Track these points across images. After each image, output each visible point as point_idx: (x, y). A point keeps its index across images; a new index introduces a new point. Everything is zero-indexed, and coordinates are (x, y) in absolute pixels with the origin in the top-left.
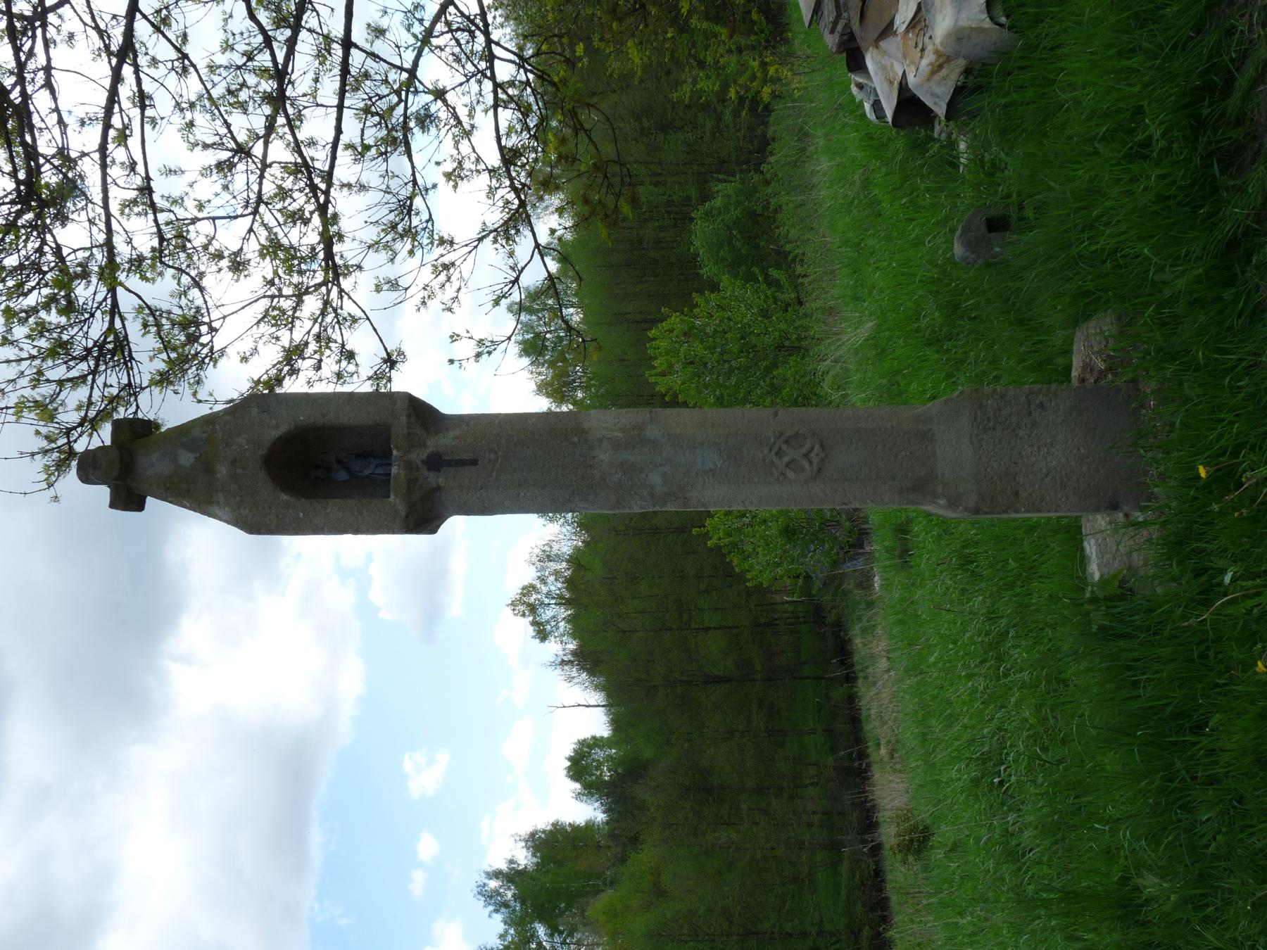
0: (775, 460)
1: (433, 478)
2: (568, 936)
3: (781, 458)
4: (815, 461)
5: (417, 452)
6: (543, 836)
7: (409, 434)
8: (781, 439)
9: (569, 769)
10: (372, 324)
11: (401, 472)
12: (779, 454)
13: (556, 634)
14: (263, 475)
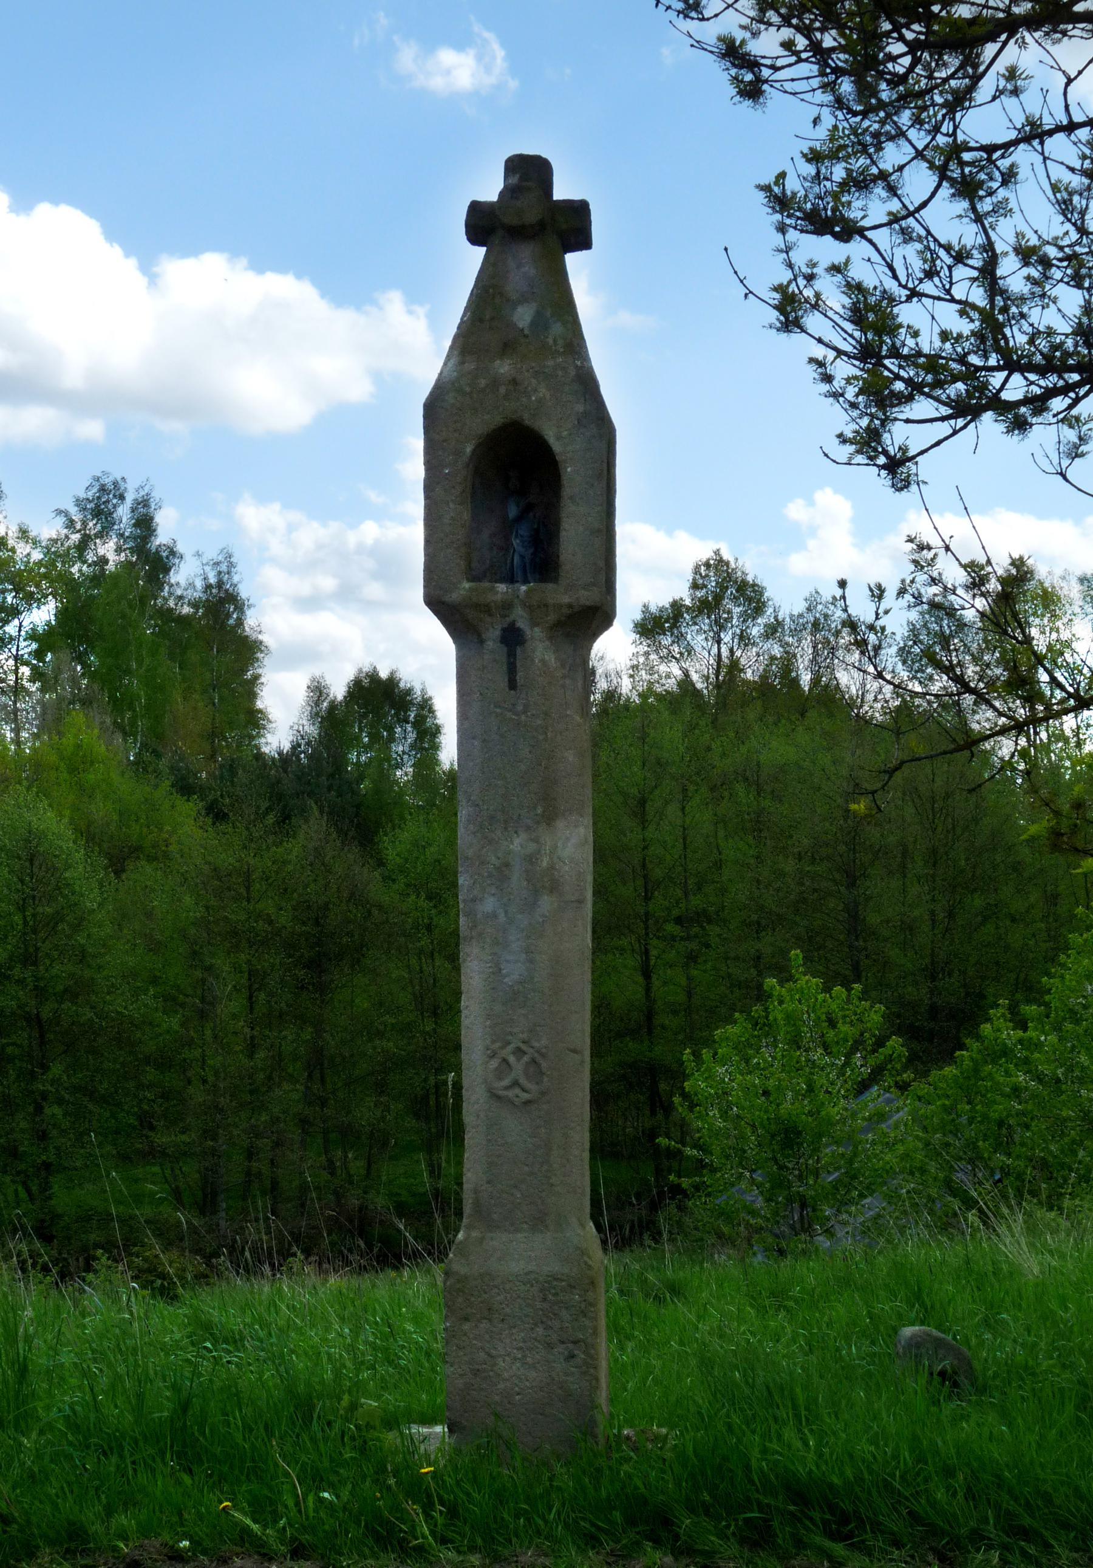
0: (510, 1048)
1: (493, 634)
2: (34, 669)
3: (514, 1053)
4: (510, 1094)
5: (525, 615)
6: (231, 622)
7: (546, 605)
8: (536, 1055)
9: (373, 676)
12: (519, 1052)
13: (653, 657)
14: (498, 420)
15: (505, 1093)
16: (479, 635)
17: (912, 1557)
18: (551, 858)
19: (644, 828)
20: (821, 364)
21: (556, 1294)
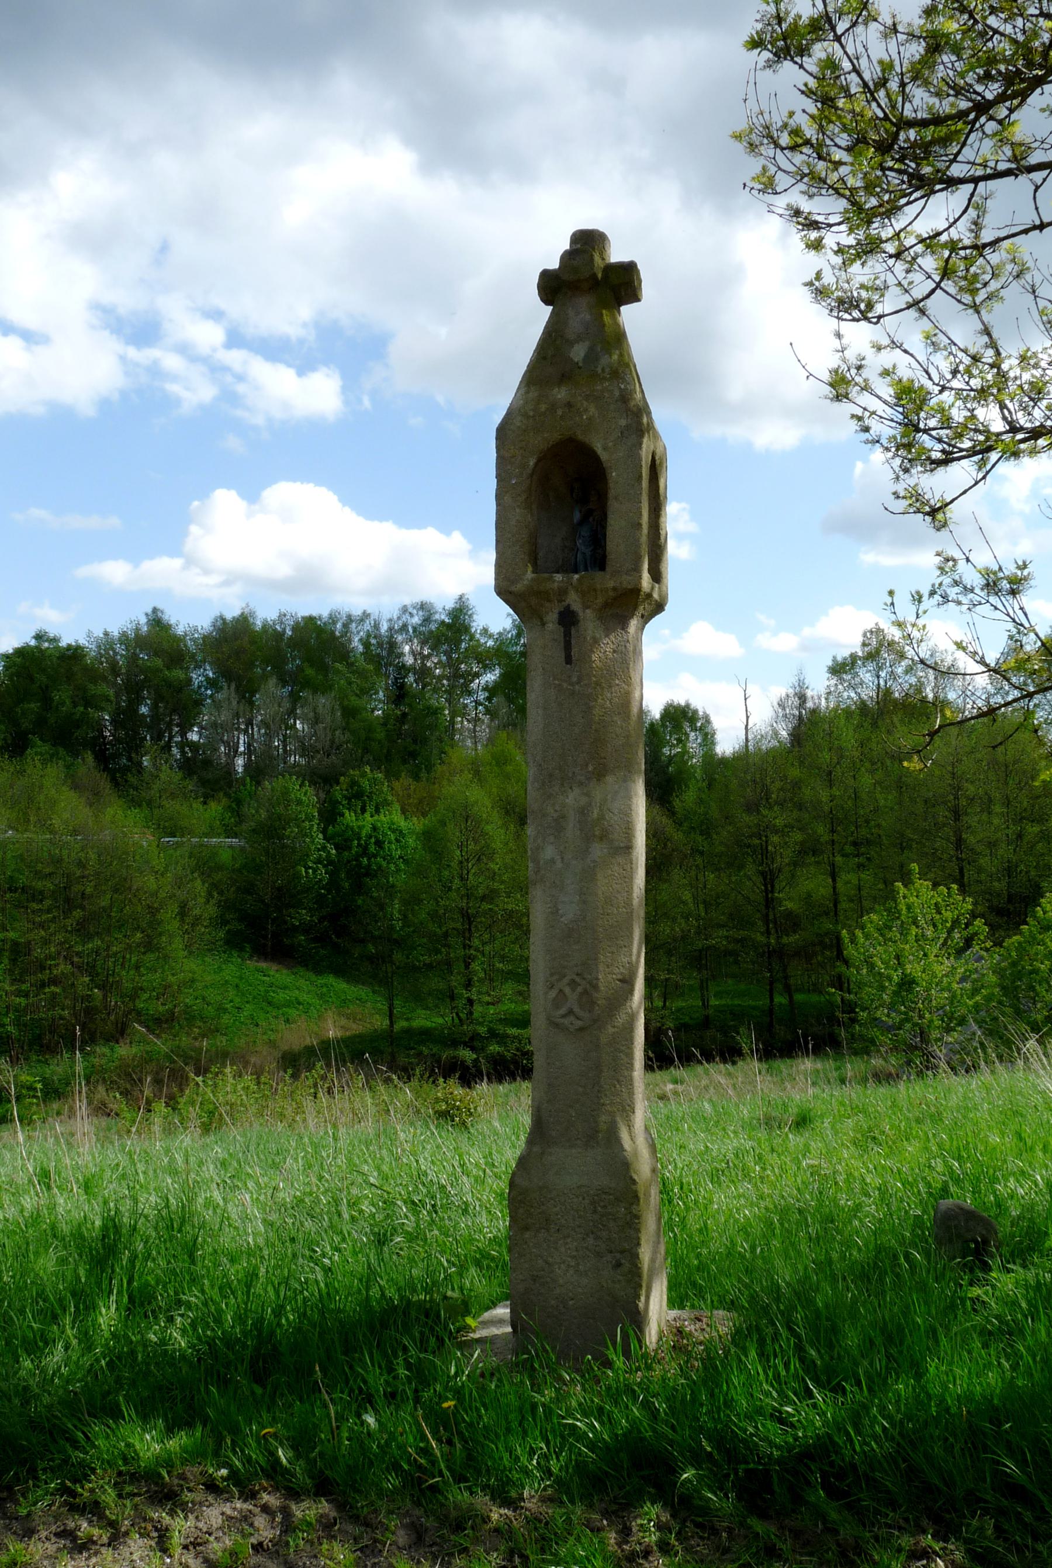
0: (566, 981)
1: (552, 617)
2: (486, 707)
3: (569, 984)
4: (566, 1021)
10: (970, 488)
11: (556, 584)
12: (573, 984)
14: (556, 436)
15: (562, 1020)
16: (542, 619)
17: (907, 1520)
18: (601, 810)
19: (831, 788)
20: (860, 419)
21: (605, 1207)
